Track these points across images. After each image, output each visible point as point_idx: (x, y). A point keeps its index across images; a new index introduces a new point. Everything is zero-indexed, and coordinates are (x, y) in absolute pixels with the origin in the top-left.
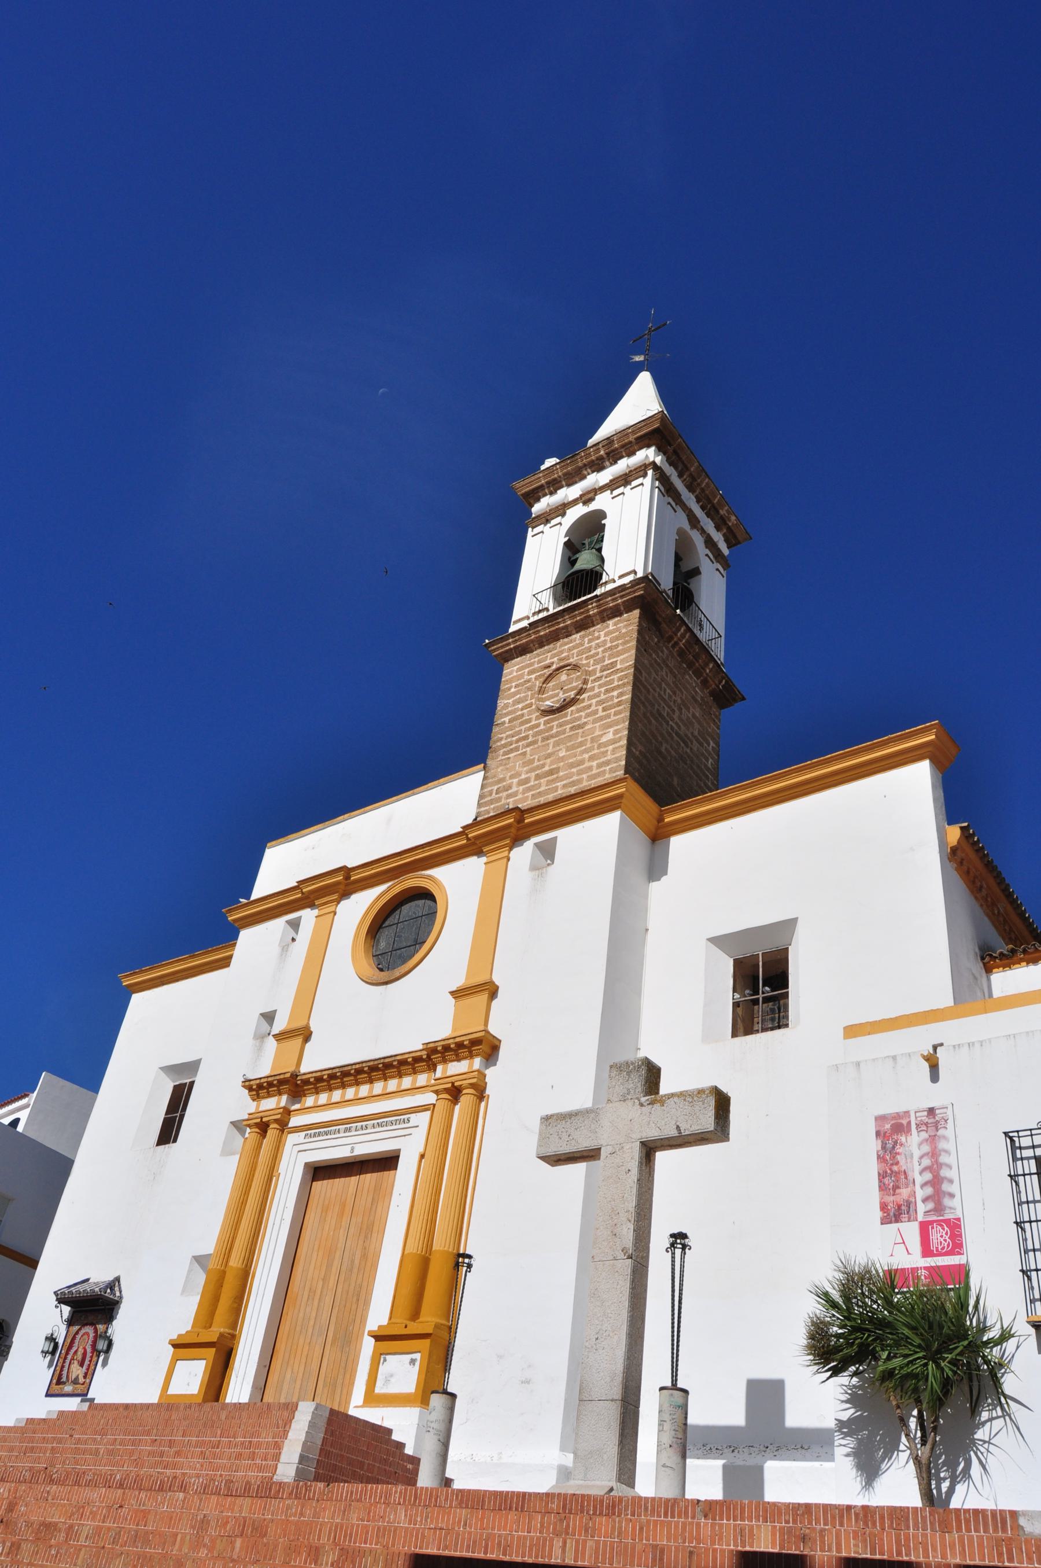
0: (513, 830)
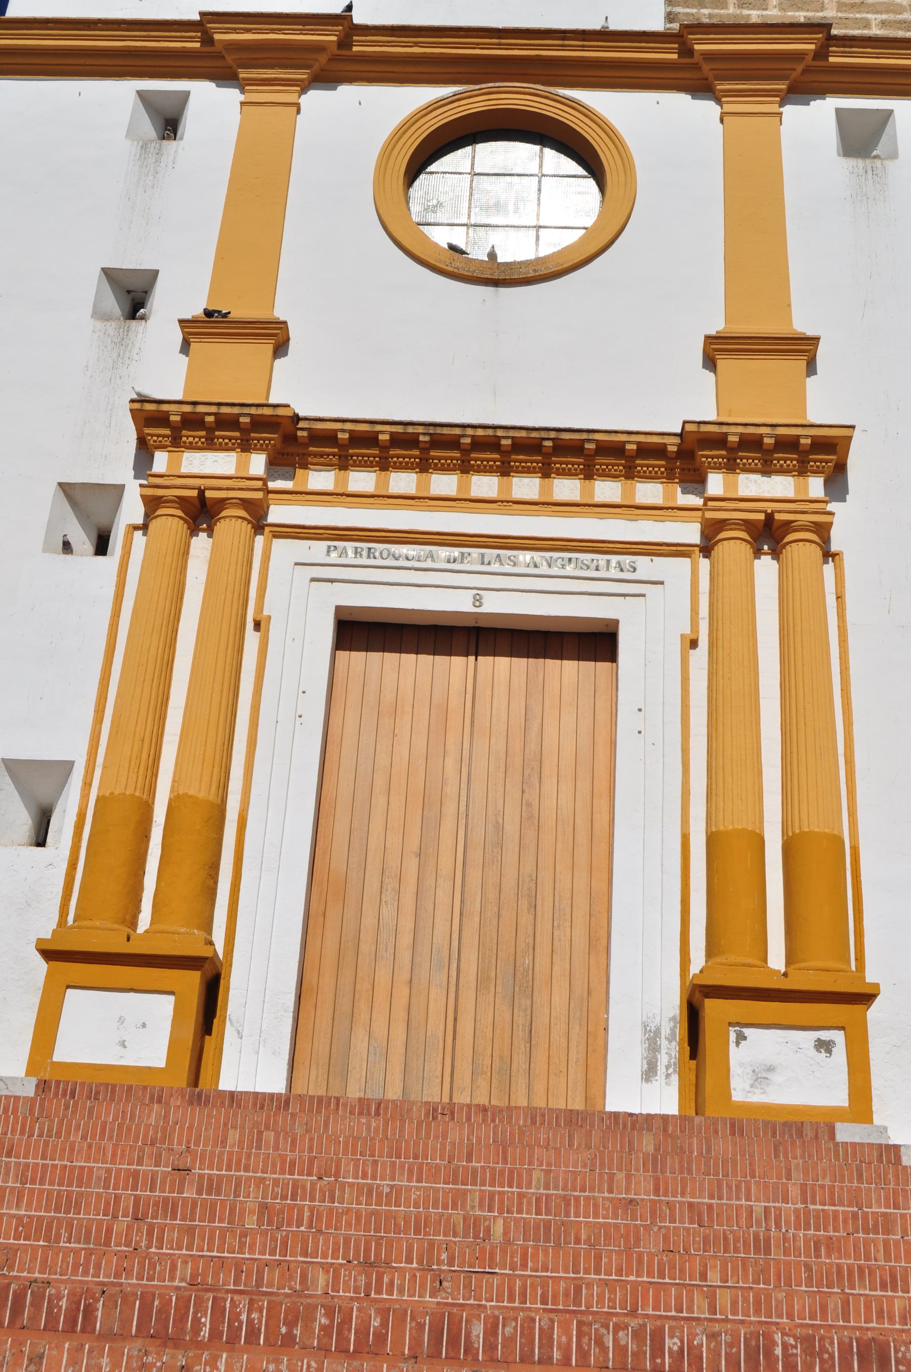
0: (323, 58)
